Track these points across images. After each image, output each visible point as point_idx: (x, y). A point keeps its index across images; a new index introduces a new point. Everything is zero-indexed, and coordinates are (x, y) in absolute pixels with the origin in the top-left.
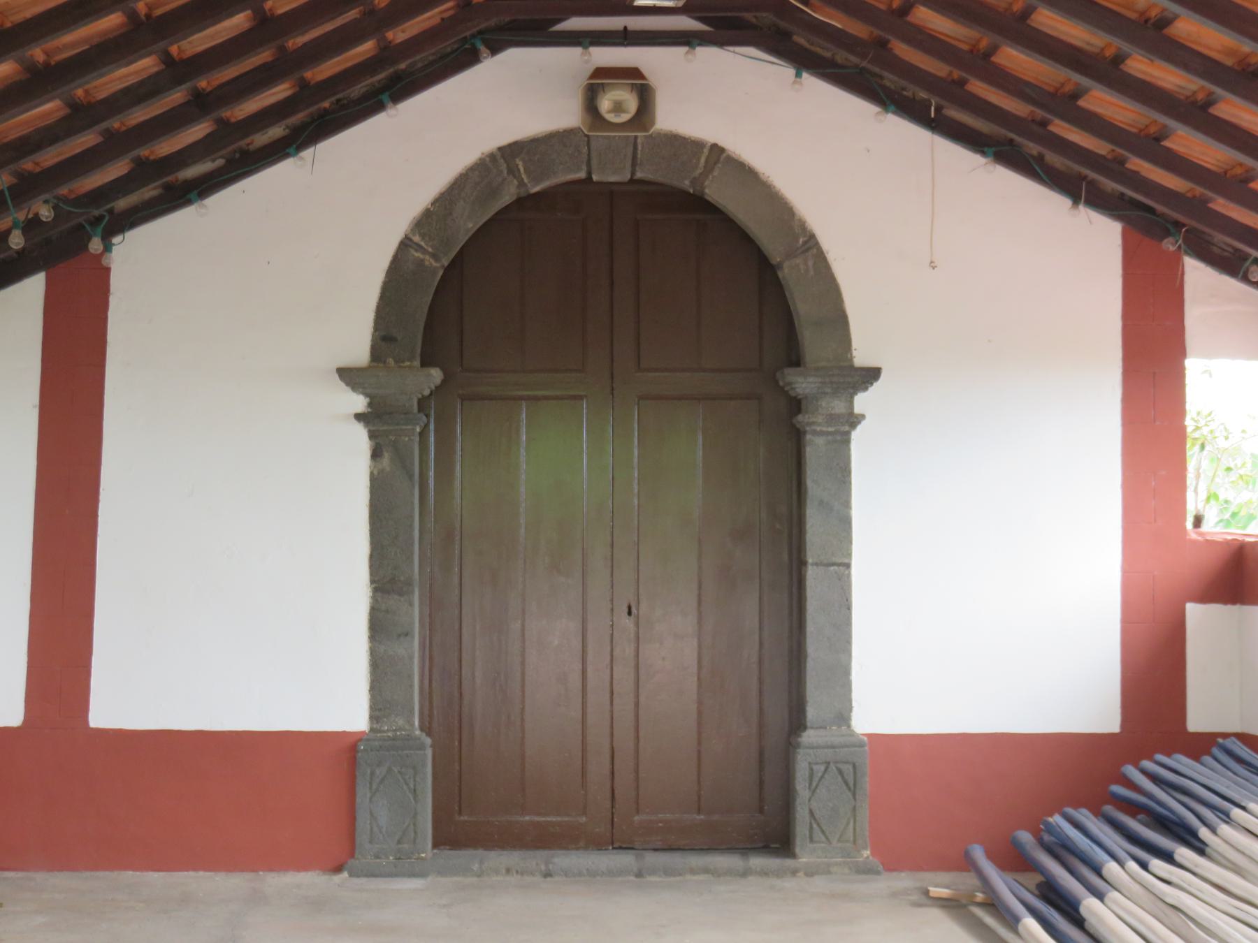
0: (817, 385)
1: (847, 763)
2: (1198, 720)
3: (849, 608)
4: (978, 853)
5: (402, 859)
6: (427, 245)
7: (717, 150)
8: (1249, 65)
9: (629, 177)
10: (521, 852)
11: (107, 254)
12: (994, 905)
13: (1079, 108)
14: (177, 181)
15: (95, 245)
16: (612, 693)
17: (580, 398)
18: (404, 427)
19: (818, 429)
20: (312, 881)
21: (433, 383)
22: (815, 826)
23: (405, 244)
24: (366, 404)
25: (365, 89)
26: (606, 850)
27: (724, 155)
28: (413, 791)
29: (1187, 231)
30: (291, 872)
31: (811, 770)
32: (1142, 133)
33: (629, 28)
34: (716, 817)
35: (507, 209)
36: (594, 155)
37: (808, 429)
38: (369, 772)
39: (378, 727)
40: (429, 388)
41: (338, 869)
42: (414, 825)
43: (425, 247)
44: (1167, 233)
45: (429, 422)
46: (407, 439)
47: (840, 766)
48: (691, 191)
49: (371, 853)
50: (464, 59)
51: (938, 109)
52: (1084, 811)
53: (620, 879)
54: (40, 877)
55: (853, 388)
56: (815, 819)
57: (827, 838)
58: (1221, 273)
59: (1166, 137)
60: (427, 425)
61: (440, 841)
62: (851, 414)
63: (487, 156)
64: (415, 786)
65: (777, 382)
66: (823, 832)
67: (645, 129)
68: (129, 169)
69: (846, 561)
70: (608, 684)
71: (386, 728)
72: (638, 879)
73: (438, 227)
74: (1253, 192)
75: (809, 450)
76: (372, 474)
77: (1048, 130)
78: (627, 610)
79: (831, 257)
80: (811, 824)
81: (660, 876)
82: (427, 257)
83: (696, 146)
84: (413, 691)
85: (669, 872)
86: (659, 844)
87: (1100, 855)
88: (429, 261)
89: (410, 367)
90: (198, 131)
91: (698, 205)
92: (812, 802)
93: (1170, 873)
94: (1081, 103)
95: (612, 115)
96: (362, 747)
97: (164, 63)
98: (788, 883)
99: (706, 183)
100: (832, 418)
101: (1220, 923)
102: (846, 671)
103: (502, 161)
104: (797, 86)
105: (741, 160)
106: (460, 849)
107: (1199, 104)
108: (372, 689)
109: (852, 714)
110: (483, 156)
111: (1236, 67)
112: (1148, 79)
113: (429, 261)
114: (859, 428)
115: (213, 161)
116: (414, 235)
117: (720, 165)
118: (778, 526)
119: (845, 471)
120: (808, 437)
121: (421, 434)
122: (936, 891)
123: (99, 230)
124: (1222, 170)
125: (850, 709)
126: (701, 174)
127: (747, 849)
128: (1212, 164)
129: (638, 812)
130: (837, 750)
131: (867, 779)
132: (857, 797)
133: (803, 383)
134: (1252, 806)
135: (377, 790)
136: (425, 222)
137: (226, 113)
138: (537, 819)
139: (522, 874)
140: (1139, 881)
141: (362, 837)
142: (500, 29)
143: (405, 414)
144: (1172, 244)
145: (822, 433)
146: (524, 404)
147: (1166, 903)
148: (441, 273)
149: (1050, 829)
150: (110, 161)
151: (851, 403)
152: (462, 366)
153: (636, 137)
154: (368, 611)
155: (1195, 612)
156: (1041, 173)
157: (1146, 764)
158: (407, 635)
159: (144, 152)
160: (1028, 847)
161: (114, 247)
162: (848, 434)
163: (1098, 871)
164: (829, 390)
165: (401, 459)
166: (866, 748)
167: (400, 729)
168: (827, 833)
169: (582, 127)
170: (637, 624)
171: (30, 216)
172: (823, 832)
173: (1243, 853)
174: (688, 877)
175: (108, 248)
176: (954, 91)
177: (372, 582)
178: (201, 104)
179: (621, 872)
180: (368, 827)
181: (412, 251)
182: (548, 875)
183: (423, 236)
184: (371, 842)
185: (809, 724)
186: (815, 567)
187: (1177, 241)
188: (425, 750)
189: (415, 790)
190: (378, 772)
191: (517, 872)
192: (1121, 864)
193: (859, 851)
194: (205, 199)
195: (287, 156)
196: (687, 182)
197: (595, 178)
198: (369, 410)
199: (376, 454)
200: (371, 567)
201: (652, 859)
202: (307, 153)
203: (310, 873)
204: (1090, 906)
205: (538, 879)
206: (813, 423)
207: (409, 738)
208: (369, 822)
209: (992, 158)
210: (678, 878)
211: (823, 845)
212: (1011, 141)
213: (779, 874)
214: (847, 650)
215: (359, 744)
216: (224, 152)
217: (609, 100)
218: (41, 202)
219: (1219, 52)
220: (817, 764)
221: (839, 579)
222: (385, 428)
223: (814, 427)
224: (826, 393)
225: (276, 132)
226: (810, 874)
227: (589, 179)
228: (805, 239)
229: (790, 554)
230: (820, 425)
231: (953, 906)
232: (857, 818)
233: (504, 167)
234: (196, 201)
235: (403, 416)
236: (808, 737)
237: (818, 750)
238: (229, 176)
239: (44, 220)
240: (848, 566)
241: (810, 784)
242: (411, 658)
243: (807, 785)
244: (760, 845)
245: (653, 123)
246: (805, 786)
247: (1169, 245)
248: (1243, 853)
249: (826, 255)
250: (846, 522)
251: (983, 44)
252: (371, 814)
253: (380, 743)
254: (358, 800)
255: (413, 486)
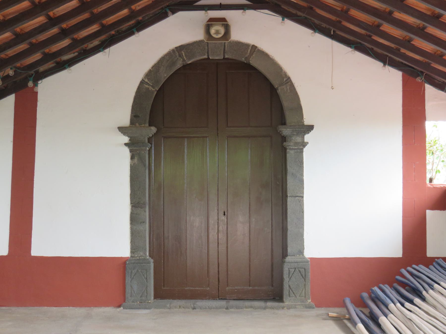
0: (291, 131)
1: (302, 268)
2: (430, 254)
3: (303, 212)
4: (348, 301)
5: (142, 303)
6: (150, 83)
7: (254, 47)
8: (435, 14)
9: (223, 57)
10: (186, 300)
11: (36, 87)
12: (350, 320)
13: (381, 30)
14: (61, 60)
15: (30, 84)
16: (218, 243)
17: (206, 137)
18: (142, 148)
19: (291, 147)
20: (109, 310)
21: (153, 132)
22: (291, 291)
23: (142, 82)
24: (128, 140)
25: (127, 27)
26: (216, 300)
27: (257, 49)
28: (146, 278)
29: (425, 74)
30: (103, 307)
31: (289, 271)
32: (404, 39)
33: (222, 4)
34: (256, 288)
35: (179, 69)
36: (210, 50)
37: (288, 147)
38: (130, 271)
39: (134, 256)
40: (151, 134)
41: (119, 306)
42: (147, 291)
43: (149, 83)
44: (418, 76)
45: (152, 146)
46: (143, 152)
47: (300, 269)
48: (246, 62)
49: (131, 301)
50: (162, 16)
51: (334, 31)
52: (387, 286)
53: (220, 310)
54: (14, 309)
55: (304, 132)
56: (291, 289)
57: (295, 295)
58: (438, 90)
59: (412, 41)
60: (151, 147)
61: (157, 296)
62: (303, 142)
63: (171, 50)
64: (147, 276)
65: (277, 131)
66: (294, 293)
67: (227, 40)
68: (42, 57)
69: (302, 195)
70: (217, 240)
71: (136, 256)
72: (227, 310)
73: (154, 76)
74: (444, 60)
75: (288, 155)
76: (131, 165)
77: (372, 38)
78: (223, 213)
79: (296, 85)
80: (289, 290)
81: (234, 309)
82: (150, 87)
83: (247, 46)
84: (146, 243)
85: (237, 307)
86: (235, 298)
87: (388, 301)
88: (151, 88)
89: (144, 126)
90: (65, 43)
91: (248, 67)
92: (289, 282)
93: (411, 307)
94: (381, 28)
95: (215, 35)
96: (128, 263)
97: (48, 19)
98: (280, 312)
99: (251, 59)
100: (296, 144)
101: (422, 325)
102: (302, 235)
103: (177, 52)
104: (283, 24)
105: (263, 50)
106: (164, 299)
107: (421, 28)
108: (132, 242)
109: (304, 251)
110: (170, 50)
111: (431, 15)
112: (402, 19)
113: (151, 88)
114: (306, 147)
115: (74, 53)
116: (145, 79)
117: (255, 53)
118: (278, 183)
119: (302, 163)
120: (288, 150)
121: (149, 150)
122: (331, 314)
123: (32, 78)
124: (434, 52)
125: (304, 249)
126: (248, 56)
127: (267, 299)
128: (429, 50)
129: (228, 286)
130: (298, 264)
131: (310, 274)
132: (306, 281)
133: (285, 131)
134: (442, 283)
135: (133, 278)
136: (149, 75)
137: (75, 36)
138: (191, 288)
139: (185, 308)
140: (400, 310)
141: (128, 295)
142: (175, 5)
143: (143, 143)
144: (420, 79)
145: (293, 149)
146: (186, 139)
147: (407, 317)
148: (155, 93)
149: (373, 292)
150: (307, 26)
151: (303, 138)
152: (164, 126)
153: (225, 43)
154: (130, 214)
155: (429, 213)
156: (372, 55)
157: (409, 269)
158: (144, 222)
159: (47, 50)
160: (365, 299)
161: (39, 85)
162: (302, 149)
163: (387, 306)
164: (295, 134)
165: (141, 159)
166: (309, 263)
167: (141, 256)
168: (295, 293)
169: (204, 39)
170: (227, 219)
171: (5, 75)
172: (294, 293)
173: (436, 300)
174: (245, 309)
175: (36, 85)
176: (337, 25)
177: (131, 203)
178: (64, 33)
179: (221, 308)
180: (130, 291)
181: (145, 85)
182: (194, 308)
183: (148, 79)
184: (131, 297)
185: (288, 254)
186: (290, 197)
187: (422, 78)
188: (150, 263)
189: (147, 278)
190: (133, 271)
191: (183, 307)
192: (395, 304)
193: (307, 300)
194: (71, 66)
195: (99, 51)
196: (243, 59)
197: (210, 58)
198: (130, 142)
199: (132, 158)
200: (131, 198)
201: (232, 303)
202: (107, 50)
203: (109, 308)
204: (383, 320)
205: (191, 310)
206: (289, 145)
207: (145, 259)
208: (130, 290)
209: (354, 49)
210: (241, 310)
211: (293, 298)
212: (360, 43)
213: (278, 308)
214: (302, 228)
215: (127, 261)
216: (77, 49)
217: (214, 30)
218: (10, 69)
219: (425, 9)
220: (291, 268)
221: (299, 202)
222: (135, 148)
223: (290, 147)
224: (294, 135)
225: (96, 42)
226: (289, 308)
227: (209, 58)
228: (286, 79)
229: (282, 193)
230: (292, 146)
231: (338, 320)
232: (306, 288)
233: (177, 54)
234: (68, 68)
235: (142, 144)
236: (288, 259)
237: (292, 264)
238: (79, 59)
239: (11, 75)
240: (302, 197)
241: (289, 276)
242: (145, 231)
243: (288, 276)
244: (272, 298)
245: (230, 38)
246: (287, 277)
247: (418, 80)
248: (436, 300)
249: (294, 85)
250: (302, 181)
251: (345, 8)
252: (131, 286)
253: (134, 261)
254: (126, 282)
255: (146, 169)
